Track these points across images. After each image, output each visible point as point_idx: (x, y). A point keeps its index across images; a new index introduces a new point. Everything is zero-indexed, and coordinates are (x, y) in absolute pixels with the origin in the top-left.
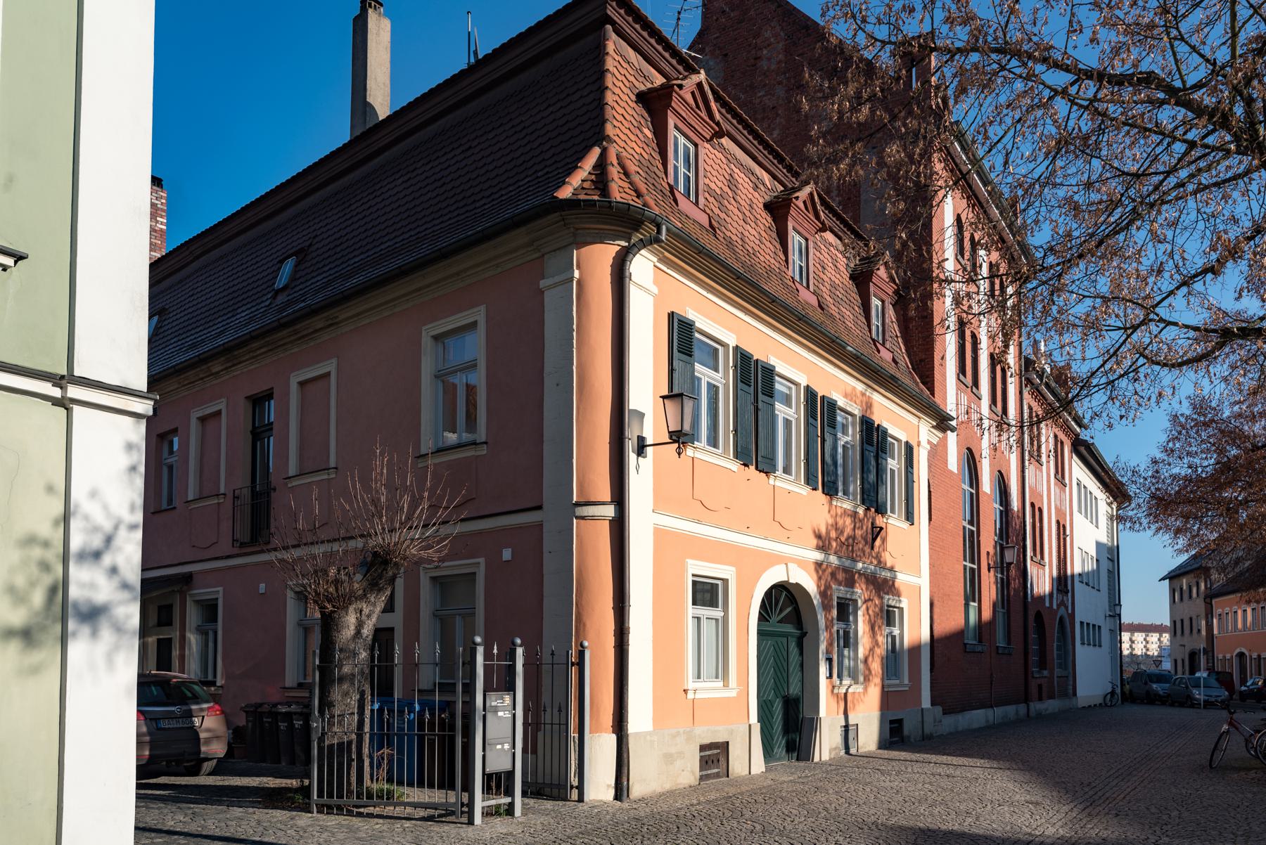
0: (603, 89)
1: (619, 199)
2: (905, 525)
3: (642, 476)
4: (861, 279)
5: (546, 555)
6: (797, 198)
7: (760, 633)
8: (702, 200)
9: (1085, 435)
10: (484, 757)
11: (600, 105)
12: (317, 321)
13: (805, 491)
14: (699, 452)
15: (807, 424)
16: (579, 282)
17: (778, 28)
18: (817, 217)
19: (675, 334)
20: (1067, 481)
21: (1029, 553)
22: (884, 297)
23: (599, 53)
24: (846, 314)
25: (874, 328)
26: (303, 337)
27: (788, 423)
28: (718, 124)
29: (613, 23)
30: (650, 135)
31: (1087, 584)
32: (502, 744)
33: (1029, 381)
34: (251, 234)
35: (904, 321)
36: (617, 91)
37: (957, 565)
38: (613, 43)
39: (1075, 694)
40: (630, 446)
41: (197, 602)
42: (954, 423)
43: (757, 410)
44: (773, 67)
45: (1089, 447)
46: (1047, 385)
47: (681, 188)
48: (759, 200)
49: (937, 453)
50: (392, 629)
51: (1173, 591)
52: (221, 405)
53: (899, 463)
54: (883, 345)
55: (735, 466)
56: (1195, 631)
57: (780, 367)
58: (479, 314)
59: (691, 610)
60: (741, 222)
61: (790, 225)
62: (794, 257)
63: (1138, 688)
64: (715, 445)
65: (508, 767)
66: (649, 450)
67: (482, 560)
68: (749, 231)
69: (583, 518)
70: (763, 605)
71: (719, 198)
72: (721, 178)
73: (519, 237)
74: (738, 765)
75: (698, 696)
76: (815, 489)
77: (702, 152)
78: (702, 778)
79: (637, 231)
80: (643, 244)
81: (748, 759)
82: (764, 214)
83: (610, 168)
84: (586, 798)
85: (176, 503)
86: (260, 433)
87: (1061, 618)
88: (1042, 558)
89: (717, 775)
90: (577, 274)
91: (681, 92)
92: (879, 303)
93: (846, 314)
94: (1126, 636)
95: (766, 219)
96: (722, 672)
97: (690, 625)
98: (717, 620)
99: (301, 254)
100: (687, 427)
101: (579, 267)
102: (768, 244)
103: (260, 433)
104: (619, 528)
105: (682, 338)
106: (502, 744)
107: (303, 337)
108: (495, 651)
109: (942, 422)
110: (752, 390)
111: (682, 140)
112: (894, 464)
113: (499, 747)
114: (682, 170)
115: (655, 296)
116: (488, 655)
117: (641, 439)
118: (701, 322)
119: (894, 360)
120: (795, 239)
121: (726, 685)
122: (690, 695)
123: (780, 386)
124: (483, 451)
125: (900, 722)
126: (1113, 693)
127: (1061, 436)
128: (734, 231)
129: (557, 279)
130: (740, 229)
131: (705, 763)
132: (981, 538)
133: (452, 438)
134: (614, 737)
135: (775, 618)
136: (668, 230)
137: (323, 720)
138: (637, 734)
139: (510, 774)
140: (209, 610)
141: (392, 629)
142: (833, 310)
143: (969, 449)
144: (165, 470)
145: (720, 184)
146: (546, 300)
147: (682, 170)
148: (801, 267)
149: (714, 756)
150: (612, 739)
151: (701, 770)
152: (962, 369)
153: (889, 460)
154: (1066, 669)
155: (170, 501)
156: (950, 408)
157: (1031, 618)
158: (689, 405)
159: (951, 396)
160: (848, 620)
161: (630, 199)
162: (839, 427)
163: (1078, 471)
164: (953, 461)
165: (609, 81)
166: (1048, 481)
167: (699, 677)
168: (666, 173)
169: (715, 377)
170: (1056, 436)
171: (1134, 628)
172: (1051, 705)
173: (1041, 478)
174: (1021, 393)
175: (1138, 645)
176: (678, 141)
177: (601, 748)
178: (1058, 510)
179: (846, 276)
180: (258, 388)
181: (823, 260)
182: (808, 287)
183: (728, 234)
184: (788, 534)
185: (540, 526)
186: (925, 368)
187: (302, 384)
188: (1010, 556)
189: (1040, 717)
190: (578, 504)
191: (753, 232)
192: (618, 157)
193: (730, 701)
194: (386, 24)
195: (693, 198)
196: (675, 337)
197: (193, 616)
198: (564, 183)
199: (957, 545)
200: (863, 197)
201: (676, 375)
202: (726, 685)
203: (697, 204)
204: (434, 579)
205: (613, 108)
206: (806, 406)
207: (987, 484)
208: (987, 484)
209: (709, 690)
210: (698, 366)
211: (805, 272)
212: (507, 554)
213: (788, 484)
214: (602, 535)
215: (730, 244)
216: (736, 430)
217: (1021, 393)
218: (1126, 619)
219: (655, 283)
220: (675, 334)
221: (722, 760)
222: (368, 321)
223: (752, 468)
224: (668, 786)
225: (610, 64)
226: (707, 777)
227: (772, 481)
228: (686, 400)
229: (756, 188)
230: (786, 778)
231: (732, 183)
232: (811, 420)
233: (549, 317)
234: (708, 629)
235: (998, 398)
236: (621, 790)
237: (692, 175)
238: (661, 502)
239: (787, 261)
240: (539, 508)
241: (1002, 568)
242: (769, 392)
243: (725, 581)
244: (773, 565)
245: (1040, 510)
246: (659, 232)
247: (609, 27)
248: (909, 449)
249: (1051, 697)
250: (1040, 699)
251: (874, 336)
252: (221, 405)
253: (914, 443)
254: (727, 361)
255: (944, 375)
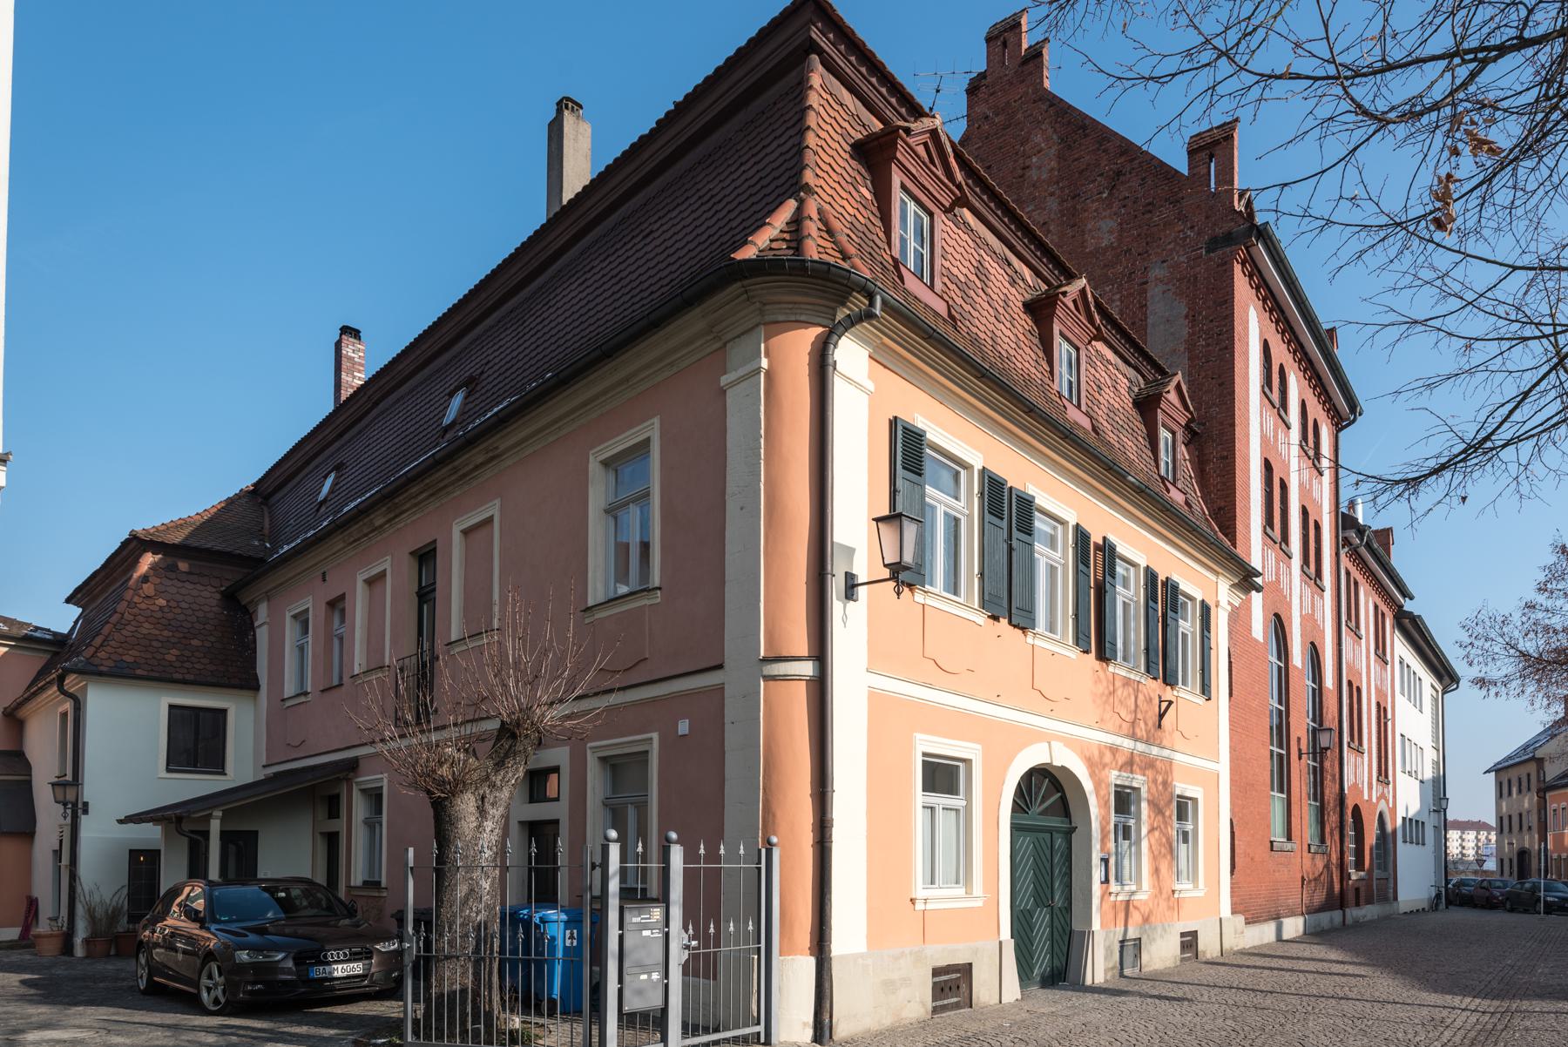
0: (803, 130)
1: (816, 257)
2: (1201, 700)
3: (850, 626)
4: (1146, 405)
5: (727, 727)
6: (1064, 294)
7: (1016, 828)
8: (938, 286)
9: (1408, 606)
10: (620, 991)
11: (800, 149)
12: (476, 455)
13: (1074, 654)
14: (933, 597)
15: (1077, 571)
16: (768, 374)
17: (1050, 130)
18: (1091, 320)
19: (899, 445)
20: (1388, 658)
21: (1346, 738)
22: (1175, 428)
23: (802, 87)
24: (1128, 444)
25: (1162, 465)
26: (465, 475)
27: (1052, 570)
28: (959, 187)
29: (820, 52)
30: (869, 196)
31: (1410, 773)
32: (649, 973)
33: (1347, 542)
34: (427, 371)
35: (1200, 465)
36: (823, 135)
37: (1263, 750)
38: (818, 77)
39: (1396, 898)
40: (836, 585)
41: (363, 791)
42: (1259, 580)
43: (1011, 549)
44: (1044, 176)
45: (1415, 621)
46: (1368, 546)
47: (911, 264)
48: (1017, 298)
49: (1239, 618)
50: (557, 822)
51: (1499, 785)
52: (386, 564)
53: (1193, 625)
54: (1174, 484)
55: (981, 618)
56: (1525, 828)
57: (1042, 500)
58: (652, 430)
59: (920, 797)
60: (993, 320)
61: (1056, 328)
62: (1062, 368)
63: (1460, 894)
64: (956, 593)
65: (657, 1002)
66: (862, 592)
67: (655, 736)
68: (1002, 330)
69: (774, 678)
70: (1020, 792)
71: (964, 287)
72: (967, 264)
73: (693, 322)
74: (984, 989)
75: (929, 907)
76: (1087, 652)
77: (939, 226)
78: (935, 1010)
79: (843, 304)
80: (852, 322)
81: (999, 983)
82: (1023, 316)
83: (808, 222)
84: (774, 1040)
85: (346, 679)
86: (426, 595)
87: (1381, 815)
88: (1361, 743)
89: (957, 1006)
90: (764, 363)
91: (910, 141)
92: (1169, 436)
93: (1128, 444)
94: (1453, 835)
95: (1025, 322)
96: (963, 875)
97: (920, 816)
98: (957, 811)
99: (471, 383)
100: (908, 558)
101: (767, 355)
102: (1028, 350)
103: (426, 595)
104: (820, 689)
105: (908, 451)
106: (649, 973)
107: (465, 475)
108: (702, 851)
109: (1246, 579)
110: (1005, 524)
111: (912, 206)
112: (1188, 626)
113: (644, 977)
114: (912, 244)
115: (870, 394)
116: (690, 856)
117: (849, 576)
118: (934, 434)
119: (1187, 503)
120: (1062, 349)
121: (969, 891)
122: (919, 906)
123: (1040, 524)
124: (658, 597)
125: (1194, 934)
126: (1438, 896)
127: (1383, 607)
128: (982, 328)
129: (741, 372)
130: (991, 327)
131: (940, 990)
132: (1292, 720)
133: (623, 590)
134: (812, 961)
135: (1036, 809)
136: (884, 302)
137: (418, 940)
138: (842, 957)
139: (665, 1010)
140: (374, 796)
141: (557, 822)
142: (1112, 438)
143: (1277, 616)
144: (336, 642)
145: (965, 271)
146: (729, 401)
147: (912, 244)
148: (1070, 383)
149: (952, 984)
150: (810, 962)
151: (934, 999)
152: (1269, 521)
153: (1181, 622)
154: (1385, 869)
155: (341, 678)
156: (1256, 562)
157: (1349, 812)
158: (910, 530)
159: (1255, 548)
160: (1129, 813)
161: (832, 258)
162: (1119, 579)
163: (1400, 648)
164: (1258, 627)
165: (812, 119)
166: (1368, 657)
167: (932, 882)
168: (889, 244)
169: (953, 504)
170: (1376, 607)
171: (1464, 826)
172: (1369, 912)
173: (1360, 654)
174: (1337, 554)
175: (1461, 845)
176: (905, 210)
177: (794, 977)
178: (1379, 691)
179: (1128, 402)
180: (420, 541)
181: (1096, 380)
182: (1079, 407)
183: (975, 330)
184: (1051, 705)
185: (720, 689)
186: (1225, 514)
187: (465, 532)
188: (1324, 740)
189: (1358, 925)
190: (766, 660)
191: (1008, 333)
192: (820, 211)
193: (974, 910)
194: (586, 129)
195: (927, 279)
196: (899, 450)
197: (359, 809)
198: (745, 243)
199: (1263, 726)
200: (1150, 321)
201: (899, 498)
202: (969, 891)
203: (931, 287)
204: (603, 760)
205: (816, 153)
206: (1076, 548)
207: (1298, 657)
208: (1298, 657)
209: (945, 897)
210: (929, 489)
211: (1075, 387)
212: (683, 727)
213: (1053, 645)
214: (798, 701)
215: (975, 341)
216: (982, 574)
217: (1337, 554)
218: (1450, 817)
219: (870, 377)
220: (899, 445)
221: (964, 986)
222: (531, 450)
223: (1004, 622)
224: (887, 1021)
225: (813, 99)
226: (944, 1008)
227: (1030, 639)
228: (906, 523)
229: (1013, 283)
230: (1045, 1010)
231: (981, 272)
232: (1081, 567)
233: (733, 422)
234: (944, 822)
235: (1312, 558)
236: (822, 1029)
237: (926, 252)
238: (878, 659)
239: (1052, 372)
240: (720, 667)
241: (1314, 753)
242: (1027, 528)
243: (967, 762)
244: (1031, 742)
245: (1359, 690)
246: (872, 304)
247: (815, 58)
248: (1206, 611)
249: (1369, 901)
250: (1357, 904)
251: (1163, 472)
252: (386, 564)
253: (1212, 604)
254: (971, 487)
255: (1248, 527)
